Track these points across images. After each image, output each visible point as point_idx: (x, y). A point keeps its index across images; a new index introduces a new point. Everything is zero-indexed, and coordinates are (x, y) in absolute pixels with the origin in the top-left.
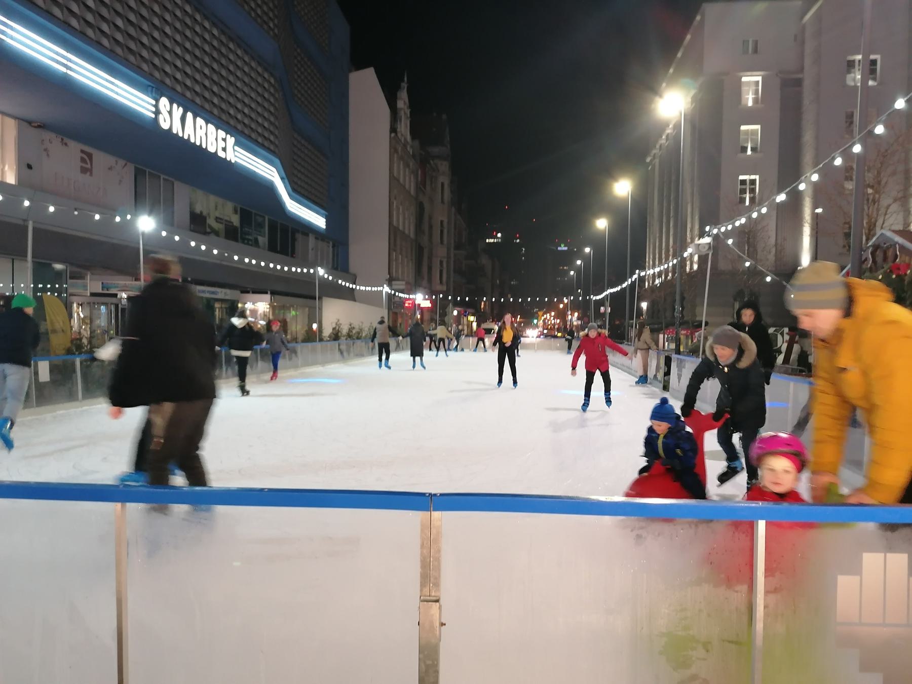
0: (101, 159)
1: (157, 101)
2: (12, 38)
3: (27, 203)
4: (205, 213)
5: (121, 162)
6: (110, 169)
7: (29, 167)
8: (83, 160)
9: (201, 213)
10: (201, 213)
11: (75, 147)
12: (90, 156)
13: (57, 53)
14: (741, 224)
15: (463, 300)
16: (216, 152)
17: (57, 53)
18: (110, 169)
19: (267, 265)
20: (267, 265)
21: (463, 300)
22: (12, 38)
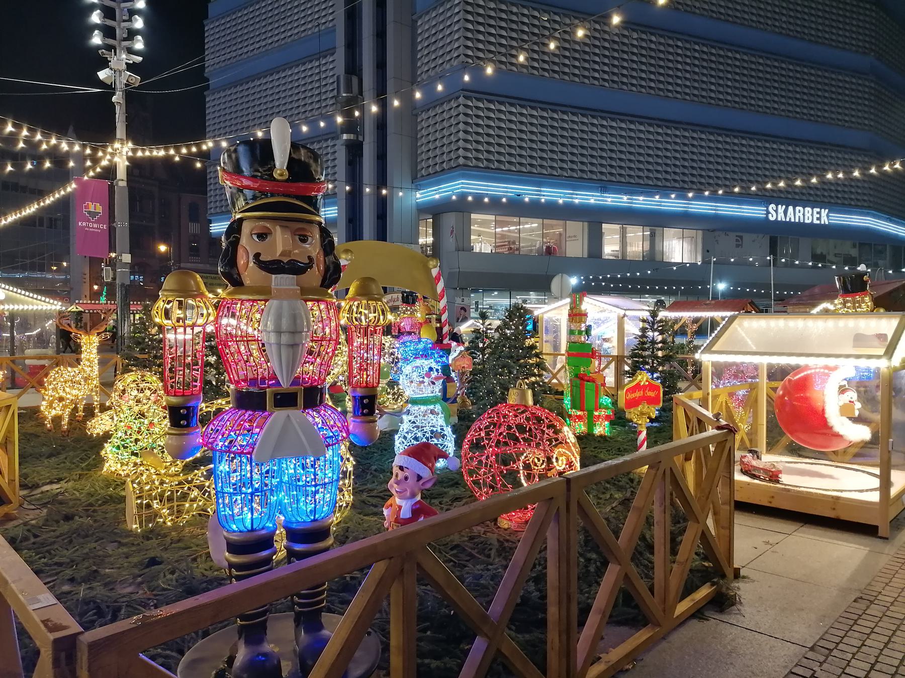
0: (747, 237)
1: (767, 208)
2: (691, 208)
3: (638, 274)
4: (824, 253)
5: (761, 236)
6: (754, 241)
7: (708, 251)
8: (737, 240)
9: (822, 253)
10: (822, 253)
11: (733, 236)
12: (741, 237)
13: (711, 206)
14: (858, 401)
15: (19, 165)
16: (804, 208)
17: (711, 206)
18: (754, 241)
19: (848, 173)
20: (848, 173)
21: (19, 165)
22: (691, 208)
